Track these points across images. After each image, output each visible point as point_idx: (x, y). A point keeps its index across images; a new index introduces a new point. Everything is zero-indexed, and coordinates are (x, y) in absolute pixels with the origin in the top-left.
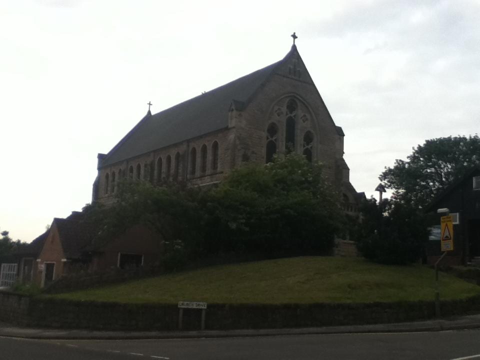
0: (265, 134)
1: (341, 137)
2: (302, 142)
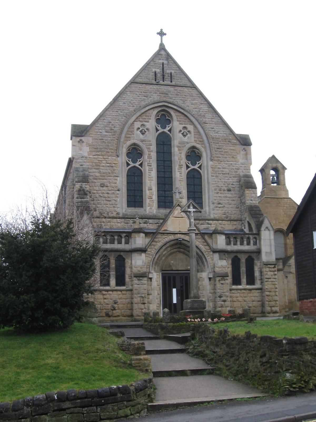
0: (123, 158)
1: (68, 213)
2: (184, 161)
